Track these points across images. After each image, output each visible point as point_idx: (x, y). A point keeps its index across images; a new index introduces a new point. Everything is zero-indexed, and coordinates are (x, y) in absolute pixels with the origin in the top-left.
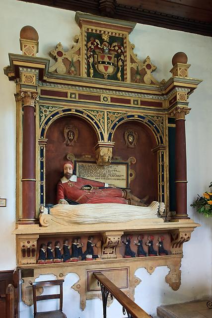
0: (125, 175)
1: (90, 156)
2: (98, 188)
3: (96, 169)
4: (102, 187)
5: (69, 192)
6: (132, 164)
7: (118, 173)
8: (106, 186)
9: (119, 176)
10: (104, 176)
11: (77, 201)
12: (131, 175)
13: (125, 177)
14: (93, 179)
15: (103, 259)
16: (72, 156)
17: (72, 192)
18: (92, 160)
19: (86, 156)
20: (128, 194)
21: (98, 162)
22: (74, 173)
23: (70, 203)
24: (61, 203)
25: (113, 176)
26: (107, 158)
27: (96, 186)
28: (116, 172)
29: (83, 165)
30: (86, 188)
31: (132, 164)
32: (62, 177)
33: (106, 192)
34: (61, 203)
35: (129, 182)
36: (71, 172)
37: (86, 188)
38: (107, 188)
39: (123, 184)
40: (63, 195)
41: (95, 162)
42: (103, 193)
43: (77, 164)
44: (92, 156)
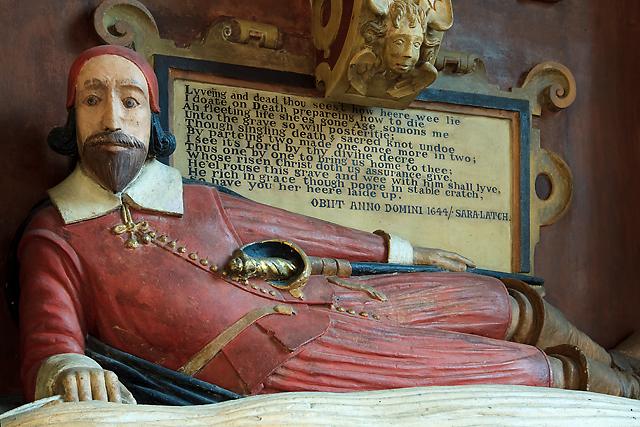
0: (505, 182)
1: (270, 34)
2: (346, 266)
3: (312, 135)
4: (372, 265)
5: (121, 298)
6: (548, 107)
7: (459, 172)
8: (401, 253)
9: (464, 191)
10: (369, 184)
11: (191, 368)
12: (545, 187)
13: (504, 202)
14: (298, 202)
15: (276, 405)
16: (135, 23)
17: (146, 293)
18: (287, 62)
19: (246, 29)
20: (552, 316)
21: (332, 78)
22: (159, 149)
23: (143, 399)
24: (61, 389)
25: (431, 189)
26: (418, 32)
27: (335, 256)
28: (447, 163)
29: (216, 103)
30: (263, 265)
31: (548, 107)
32: (60, 176)
33: (409, 299)
34: (61, 389)
35: (77, 300)
36: (134, 125)
37: (263, 265)
38: (402, 270)
39: (493, 249)
40: (70, 320)
41: (306, 83)
42: (392, 307)
43: (178, 89)
44: (284, 36)
